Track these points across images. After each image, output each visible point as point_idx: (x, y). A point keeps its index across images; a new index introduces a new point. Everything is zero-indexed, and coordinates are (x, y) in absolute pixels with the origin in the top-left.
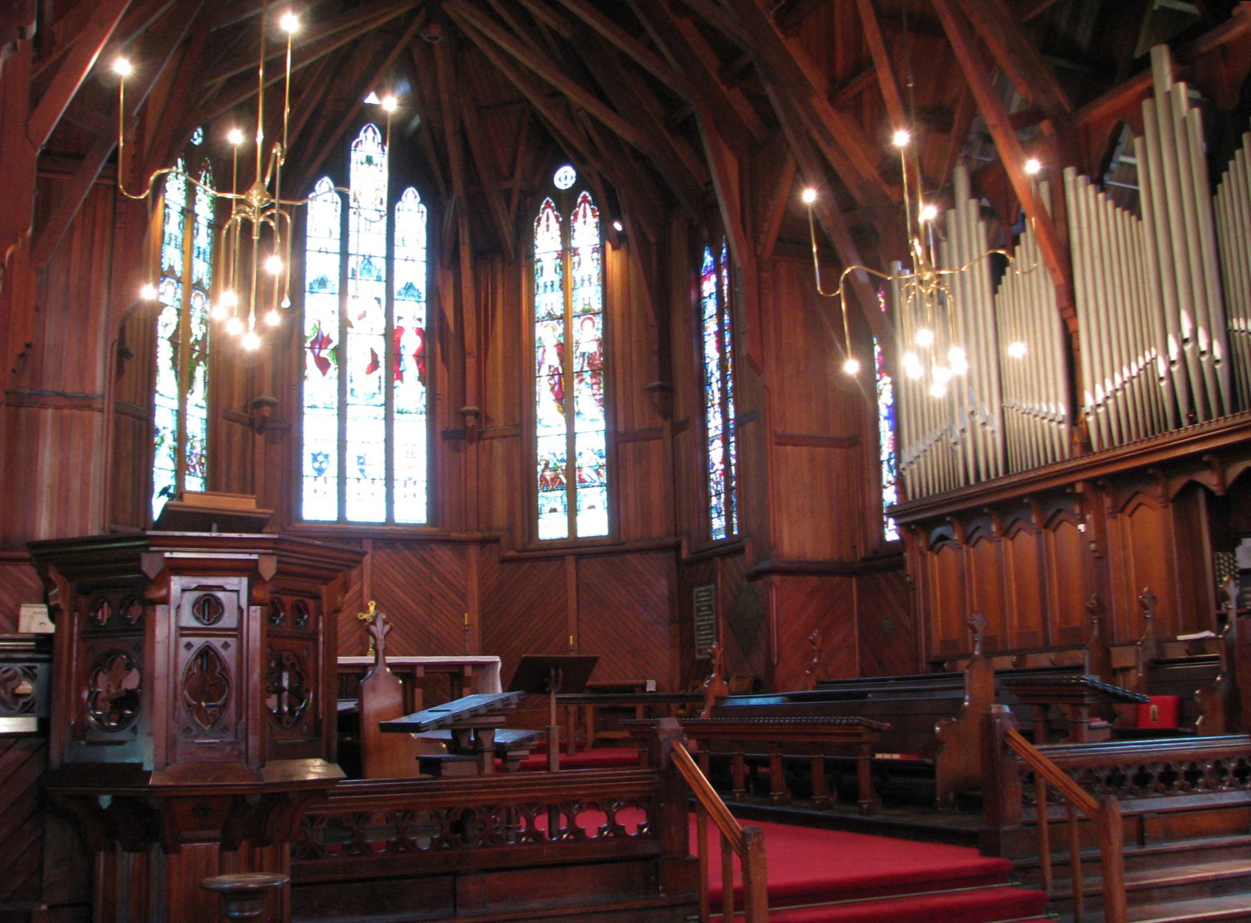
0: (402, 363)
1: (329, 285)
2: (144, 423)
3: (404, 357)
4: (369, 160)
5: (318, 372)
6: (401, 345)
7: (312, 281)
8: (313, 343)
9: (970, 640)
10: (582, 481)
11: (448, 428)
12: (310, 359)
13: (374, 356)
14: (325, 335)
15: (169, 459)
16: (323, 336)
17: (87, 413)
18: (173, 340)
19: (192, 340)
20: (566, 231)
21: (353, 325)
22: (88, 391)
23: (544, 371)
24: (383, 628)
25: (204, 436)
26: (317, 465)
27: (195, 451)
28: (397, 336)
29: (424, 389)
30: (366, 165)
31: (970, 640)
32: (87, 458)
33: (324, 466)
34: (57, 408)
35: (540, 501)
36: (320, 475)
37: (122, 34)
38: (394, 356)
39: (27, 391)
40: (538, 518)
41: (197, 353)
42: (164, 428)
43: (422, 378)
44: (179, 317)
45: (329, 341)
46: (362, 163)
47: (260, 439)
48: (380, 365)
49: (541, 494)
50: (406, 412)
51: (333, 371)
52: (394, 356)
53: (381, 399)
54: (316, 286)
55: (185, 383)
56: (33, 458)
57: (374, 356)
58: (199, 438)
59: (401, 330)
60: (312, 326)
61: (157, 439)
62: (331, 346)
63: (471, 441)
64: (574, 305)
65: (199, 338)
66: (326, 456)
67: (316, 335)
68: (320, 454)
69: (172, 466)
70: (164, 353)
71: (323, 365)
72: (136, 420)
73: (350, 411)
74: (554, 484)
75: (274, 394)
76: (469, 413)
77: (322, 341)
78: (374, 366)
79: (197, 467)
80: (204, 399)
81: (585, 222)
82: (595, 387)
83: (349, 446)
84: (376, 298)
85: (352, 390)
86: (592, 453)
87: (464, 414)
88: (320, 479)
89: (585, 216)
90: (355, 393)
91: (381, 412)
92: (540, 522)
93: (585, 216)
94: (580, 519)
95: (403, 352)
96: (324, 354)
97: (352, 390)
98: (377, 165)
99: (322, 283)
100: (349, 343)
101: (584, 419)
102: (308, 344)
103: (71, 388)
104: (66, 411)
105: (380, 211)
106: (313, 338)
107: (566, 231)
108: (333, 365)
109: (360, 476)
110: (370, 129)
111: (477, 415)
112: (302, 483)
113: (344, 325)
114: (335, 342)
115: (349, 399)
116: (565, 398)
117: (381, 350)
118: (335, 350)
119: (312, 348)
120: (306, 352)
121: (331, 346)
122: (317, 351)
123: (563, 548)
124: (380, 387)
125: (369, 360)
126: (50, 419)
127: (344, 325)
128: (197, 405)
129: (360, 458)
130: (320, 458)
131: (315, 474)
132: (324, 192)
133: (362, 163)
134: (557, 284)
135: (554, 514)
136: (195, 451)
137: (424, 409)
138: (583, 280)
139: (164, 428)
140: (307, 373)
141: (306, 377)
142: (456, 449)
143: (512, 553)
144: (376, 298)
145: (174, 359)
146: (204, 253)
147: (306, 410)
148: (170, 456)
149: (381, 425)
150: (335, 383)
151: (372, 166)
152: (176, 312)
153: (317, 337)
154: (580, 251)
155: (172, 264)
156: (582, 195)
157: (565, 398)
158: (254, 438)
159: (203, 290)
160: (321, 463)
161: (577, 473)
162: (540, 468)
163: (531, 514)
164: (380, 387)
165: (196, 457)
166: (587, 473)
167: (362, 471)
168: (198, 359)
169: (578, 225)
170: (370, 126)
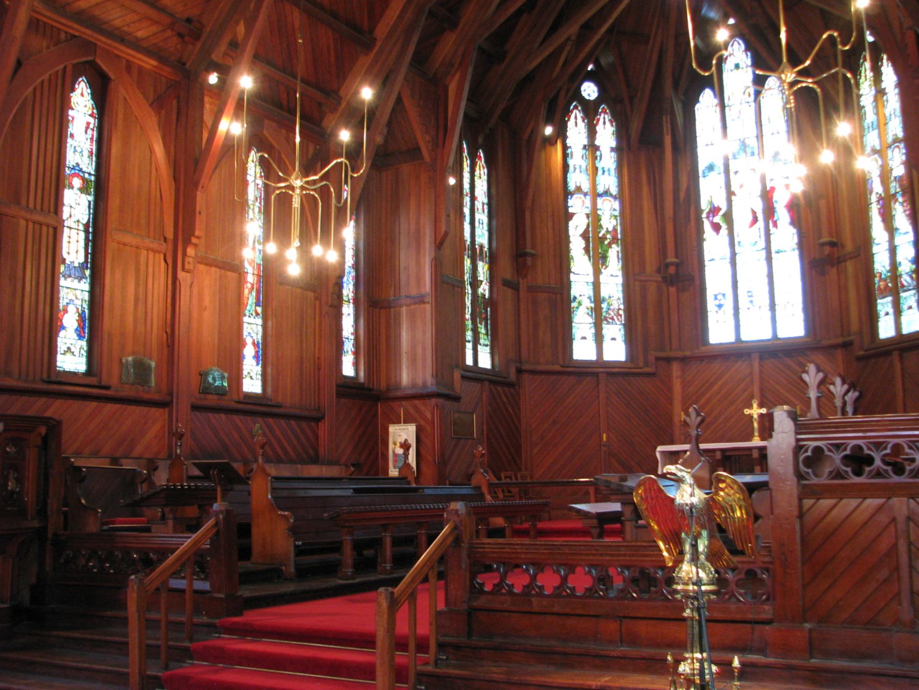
0: (776, 214)
1: (716, 169)
2: (559, 296)
3: (777, 209)
4: (737, 66)
5: (714, 233)
6: (774, 200)
7: (704, 169)
8: (708, 213)
9: (174, 444)
10: (903, 286)
11: (814, 258)
12: (707, 226)
13: (754, 213)
14: (716, 206)
15: (588, 316)
16: (714, 207)
17: (422, 306)
18: (585, 236)
19: (603, 232)
20: (592, 132)
21: (736, 193)
22: (423, 292)
23: (874, 198)
24: (696, 419)
25: (621, 295)
26: (717, 302)
27: (612, 307)
28: (770, 195)
29: (795, 231)
30: (735, 71)
31: (174, 444)
32: (424, 332)
33: (722, 302)
34: (408, 305)
35: (879, 307)
36: (720, 309)
37: (368, 72)
38: (769, 211)
39: (393, 298)
40: (878, 321)
41: (609, 240)
42: (581, 296)
43: (793, 223)
44: (588, 219)
45: (719, 209)
46: (732, 71)
47: (673, 290)
48: (759, 219)
49: (879, 301)
50: (782, 252)
51: (724, 230)
52: (769, 211)
53: (763, 244)
54: (706, 171)
55: (599, 260)
56: (398, 337)
57: (754, 213)
58: (616, 298)
59: (773, 189)
60: (707, 202)
61: (574, 305)
62: (721, 213)
63: (832, 265)
64: (598, 187)
65: (610, 229)
66: (724, 295)
67: (709, 207)
68: (720, 294)
69: (591, 320)
70: (577, 246)
71: (716, 228)
72: (551, 295)
73: (738, 258)
74: (885, 293)
75: (676, 257)
76: (672, 264)
77: (714, 211)
78: (755, 220)
79: (615, 318)
80: (874, 239)
81: (604, 128)
82: (905, 205)
83: (739, 284)
84: (752, 169)
85: (739, 242)
86: (907, 261)
87: (667, 265)
88: (721, 312)
89: (604, 123)
90: (741, 244)
91: (763, 254)
92: (880, 324)
93: (604, 123)
94: (904, 319)
95: (775, 205)
96: (718, 219)
97: (739, 242)
98: (743, 68)
99: (711, 168)
100: (733, 208)
101: (900, 233)
102: (704, 215)
103: (414, 292)
104: (413, 307)
105: (748, 102)
106: (707, 210)
107: (592, 132)
108: (724, 226)
109: (749, 305)
110: (736, 43)
111: (677, 265)
112: (707, 317)
113: (730, 194)
114: (724, 209)
115: (737, 249)
116: (887, 218)
117: (759, 207)
118: (724, 215)
119: (708, 217)
120: (703, 222)
121: (721, 213)
122: (711, 218)
123: (482, 374)
124: (760, 237)
125: (750, 218)
126: (404, 312)
127: (730, 194)
128: (612, 275)
129: (749, 292)
130: (719, 297)
131: (717, 309)
132: (707, 98)
133: (732, 71)
134: (600, 172)
135: (584, 341)
136: (612, 307)
137: (796, 247)
138: (869, 127)
139: (581, 296)
140: (705, 236)
141: (704, 240)
142: (823, 273)
143: (862, 353)
144: (752, 169)
145: (587, 250)
146: (609, 170)
147: (706, 263)
148: (588, 314)
149: (764, 264)
150: (726, 239)
151: (739, 70)
152: (585, 216)
153: (710, 209)
154: (601, 148)
155: (578, 185)
156: (601, 107)
157: (887, 218)
158: (668, 290)
159: (611, 195)
160: (720, 300)
161: (899, 279)
162: (877, 280)
163: (872, 318)
164: (760, 237)
165: (613, 312)
166: (906, 280)
167: (751, 302)
168: (610, 245)
169: (599, 128)
170: (735, 40)
